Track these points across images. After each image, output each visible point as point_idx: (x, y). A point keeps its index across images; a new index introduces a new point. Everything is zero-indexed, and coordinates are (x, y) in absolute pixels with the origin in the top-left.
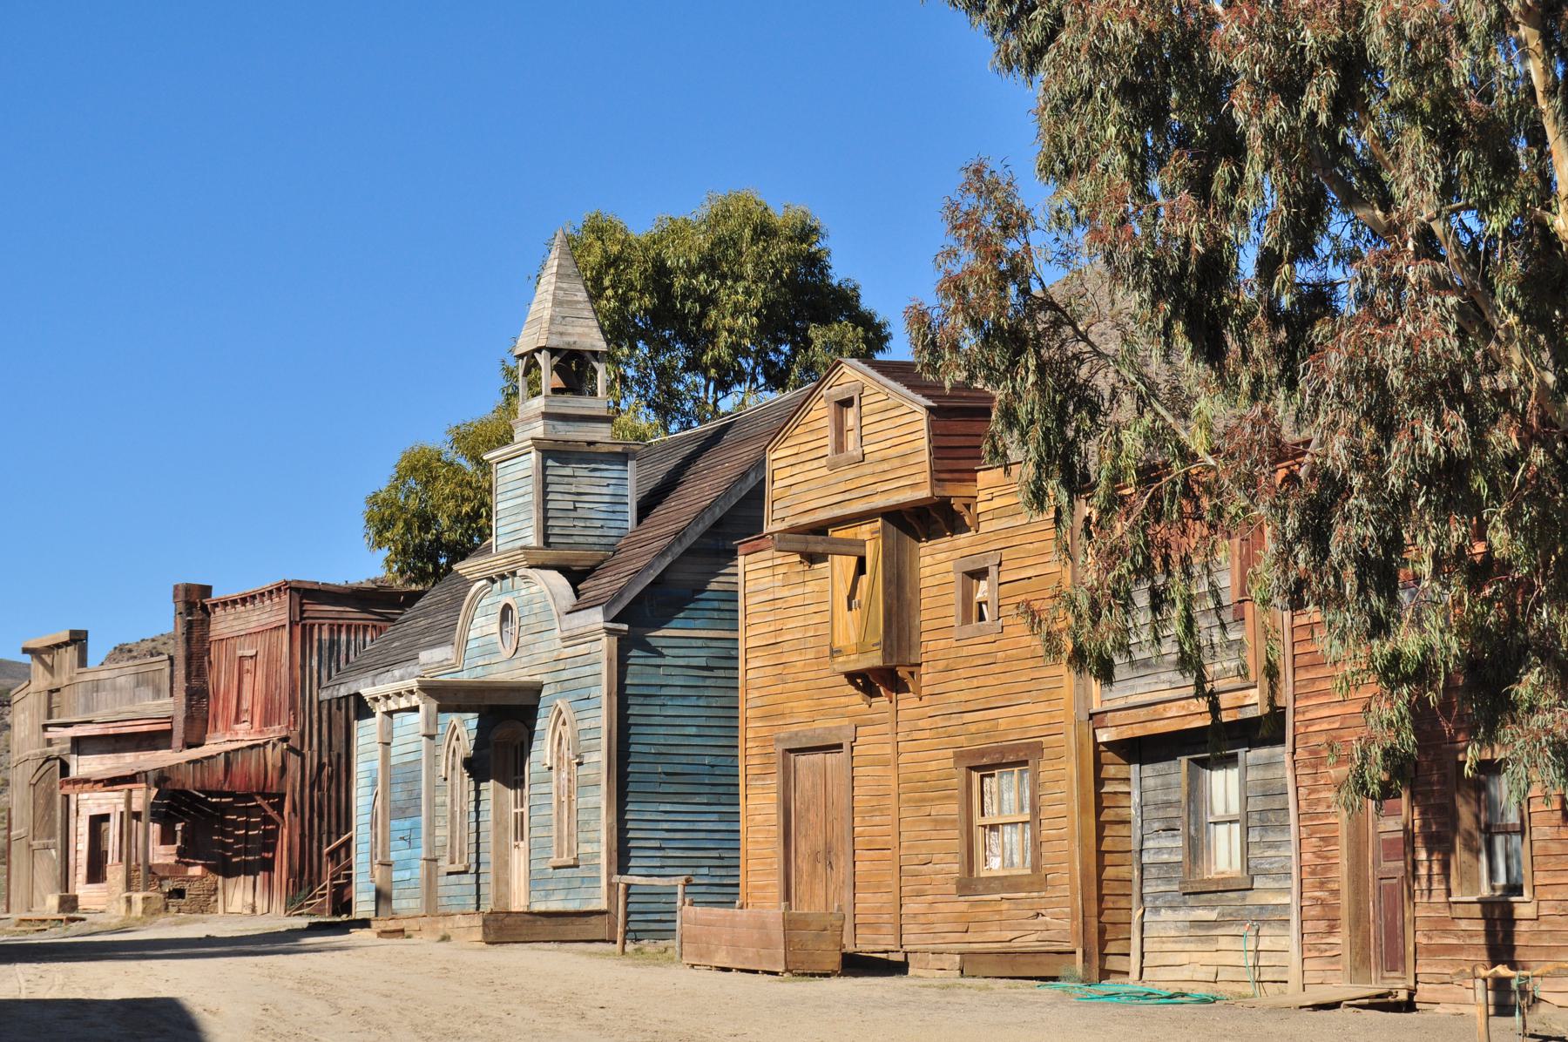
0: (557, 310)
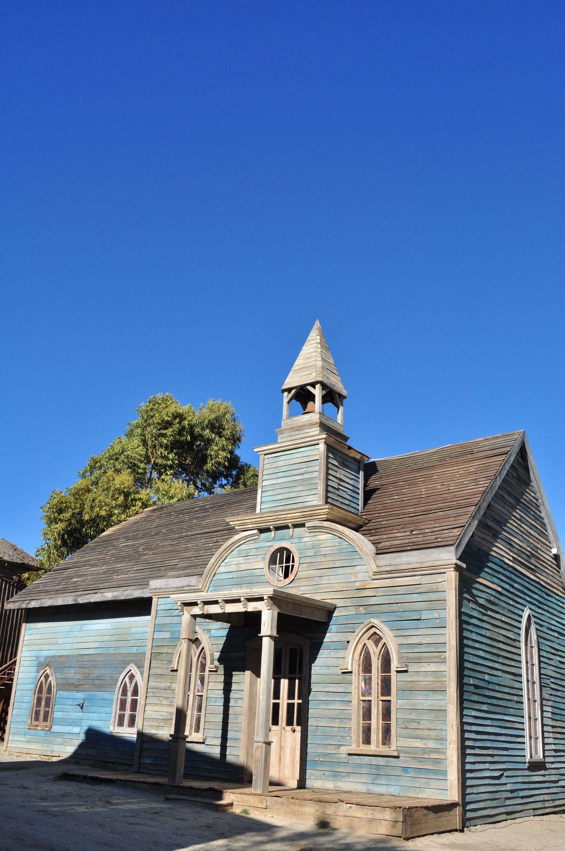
0: (324, 363)
